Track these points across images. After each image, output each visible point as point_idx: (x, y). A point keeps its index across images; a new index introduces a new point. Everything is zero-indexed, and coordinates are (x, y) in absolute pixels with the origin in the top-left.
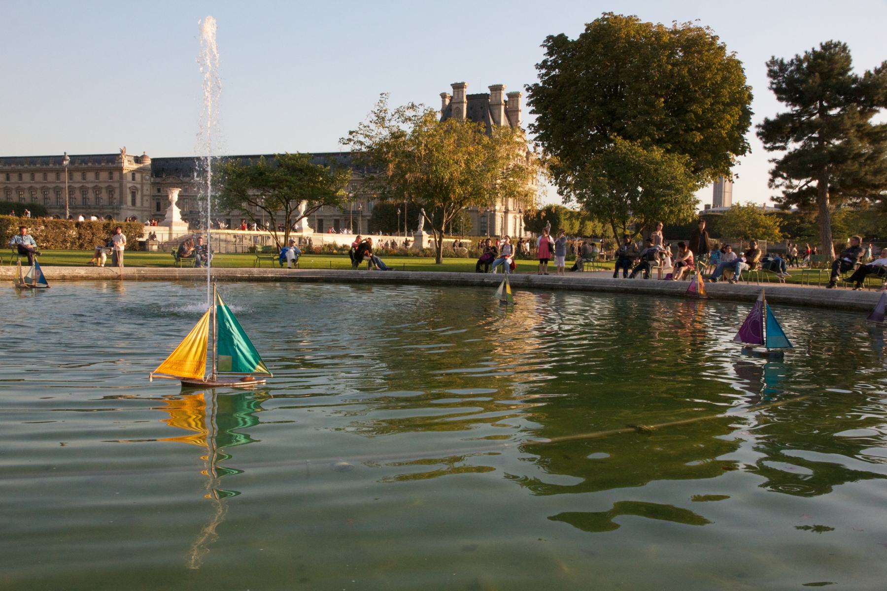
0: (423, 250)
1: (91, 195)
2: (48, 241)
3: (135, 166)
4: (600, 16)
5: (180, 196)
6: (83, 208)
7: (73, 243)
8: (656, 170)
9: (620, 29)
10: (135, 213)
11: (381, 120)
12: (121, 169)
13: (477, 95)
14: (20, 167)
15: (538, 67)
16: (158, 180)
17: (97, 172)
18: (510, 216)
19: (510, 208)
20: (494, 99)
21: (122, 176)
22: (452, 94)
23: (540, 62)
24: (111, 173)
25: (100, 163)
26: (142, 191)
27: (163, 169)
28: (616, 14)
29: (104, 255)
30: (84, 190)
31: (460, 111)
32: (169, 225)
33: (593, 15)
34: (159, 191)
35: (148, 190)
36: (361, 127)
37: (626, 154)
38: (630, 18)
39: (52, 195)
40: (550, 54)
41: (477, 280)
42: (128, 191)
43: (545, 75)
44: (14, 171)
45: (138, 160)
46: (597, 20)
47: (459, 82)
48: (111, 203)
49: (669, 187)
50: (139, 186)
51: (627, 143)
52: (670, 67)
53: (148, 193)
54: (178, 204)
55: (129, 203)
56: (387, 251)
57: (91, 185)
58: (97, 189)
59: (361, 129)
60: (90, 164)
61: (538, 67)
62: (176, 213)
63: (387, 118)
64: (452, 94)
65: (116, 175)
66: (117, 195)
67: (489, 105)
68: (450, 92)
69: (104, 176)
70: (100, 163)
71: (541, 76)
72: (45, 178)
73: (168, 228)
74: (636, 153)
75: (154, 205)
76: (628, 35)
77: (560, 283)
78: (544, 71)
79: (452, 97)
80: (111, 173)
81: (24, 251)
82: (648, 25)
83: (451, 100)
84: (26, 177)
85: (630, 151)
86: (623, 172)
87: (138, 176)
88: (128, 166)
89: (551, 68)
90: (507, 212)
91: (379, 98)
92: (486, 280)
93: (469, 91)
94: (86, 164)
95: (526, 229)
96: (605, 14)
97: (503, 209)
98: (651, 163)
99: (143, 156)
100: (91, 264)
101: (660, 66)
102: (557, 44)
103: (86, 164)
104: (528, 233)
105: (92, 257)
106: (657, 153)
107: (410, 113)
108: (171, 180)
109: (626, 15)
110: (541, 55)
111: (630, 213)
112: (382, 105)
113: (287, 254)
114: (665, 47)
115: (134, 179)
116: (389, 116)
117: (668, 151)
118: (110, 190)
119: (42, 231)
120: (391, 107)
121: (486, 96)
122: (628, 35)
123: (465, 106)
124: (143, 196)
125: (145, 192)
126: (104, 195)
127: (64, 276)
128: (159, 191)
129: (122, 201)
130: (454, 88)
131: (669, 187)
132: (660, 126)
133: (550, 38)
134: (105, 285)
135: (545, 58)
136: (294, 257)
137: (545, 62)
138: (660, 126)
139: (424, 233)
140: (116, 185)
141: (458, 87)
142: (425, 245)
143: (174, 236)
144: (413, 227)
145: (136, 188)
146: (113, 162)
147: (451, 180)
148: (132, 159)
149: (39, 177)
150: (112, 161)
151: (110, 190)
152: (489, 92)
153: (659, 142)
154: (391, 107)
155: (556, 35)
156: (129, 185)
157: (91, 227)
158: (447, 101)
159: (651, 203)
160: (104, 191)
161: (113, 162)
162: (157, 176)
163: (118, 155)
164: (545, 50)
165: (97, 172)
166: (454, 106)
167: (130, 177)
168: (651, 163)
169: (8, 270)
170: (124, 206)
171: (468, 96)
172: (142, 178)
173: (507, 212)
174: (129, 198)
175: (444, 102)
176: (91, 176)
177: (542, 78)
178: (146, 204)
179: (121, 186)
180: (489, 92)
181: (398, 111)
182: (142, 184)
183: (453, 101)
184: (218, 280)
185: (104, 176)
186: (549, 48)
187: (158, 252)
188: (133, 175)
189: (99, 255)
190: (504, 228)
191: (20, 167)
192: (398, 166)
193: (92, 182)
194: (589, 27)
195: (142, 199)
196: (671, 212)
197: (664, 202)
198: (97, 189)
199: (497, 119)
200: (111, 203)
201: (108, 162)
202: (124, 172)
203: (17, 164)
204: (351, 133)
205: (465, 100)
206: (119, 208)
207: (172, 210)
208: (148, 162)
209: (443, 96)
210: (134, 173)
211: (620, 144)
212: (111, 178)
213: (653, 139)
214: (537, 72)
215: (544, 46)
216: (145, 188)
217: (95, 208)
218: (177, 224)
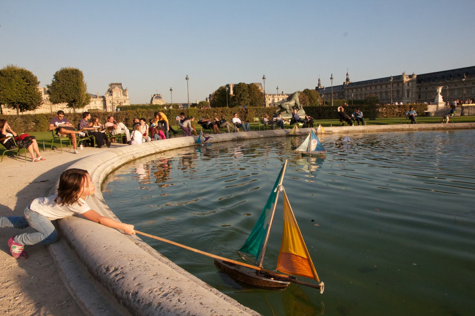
3: (409, 79)
5: (442, 90)
7: (397, 114)
10: (409, 101)
12: (403, 81)
14: (361, 86)
16: (420, 85)
24: (398, 84)
25: (382, 81)
26: (412, 90)
27: (422, 80)
29: (448, 118)
30: (386, 92)
32: (437, 104)
34: (420, 89)
35: (415, 89)
39: (384, 95)
42: (406, 91)
44: (359, 87)
45: (410, 77)
48: (398, 97)
50: (410, 88)
53: (415, 91)
54: (441, 94)
55: (406, 96)
57: (374, 92)
58: (381, 93)
62: (440, 98)
65: (401, 85)
66: (401, 93)
72: (371, 89)
75: (418, 96)
80: (398, 84)
81: (411, 117)
84: (364, 89)
87: (410, 84)
88: (406, 79)
99: (413, 75)
105: (441, 119)
108: (440, 82)
115: (408, 85)
118: (398, 92)
124: (412, 92)
125: (414, 91)
128: (420, 89)
129: (403, 95)
134: (447, 132)
140: (400, 89)
144: (210, 129)
145: (409, 89)
148: (408, 77)
149: (373, 88)
151: (398, 92)
156: (406, 88)
161: (399, 79)
162: (419, 83)
167: (406, 84)
172: (412, 85)
174: (406, 94)
176: (379, 87)
178: (414, 96)
179: (403, 89)
187: (435, 116)
189: (445, 118)
191: (361, 86)
195: (412, 94)
198: (381, 93)
200: (398, 97)
201: (397, 79)
203: (360, 84)
207: (438, 97)
210: (408, 82)
212: (398, 86)
216: (413, 89)
218: (441, 103)
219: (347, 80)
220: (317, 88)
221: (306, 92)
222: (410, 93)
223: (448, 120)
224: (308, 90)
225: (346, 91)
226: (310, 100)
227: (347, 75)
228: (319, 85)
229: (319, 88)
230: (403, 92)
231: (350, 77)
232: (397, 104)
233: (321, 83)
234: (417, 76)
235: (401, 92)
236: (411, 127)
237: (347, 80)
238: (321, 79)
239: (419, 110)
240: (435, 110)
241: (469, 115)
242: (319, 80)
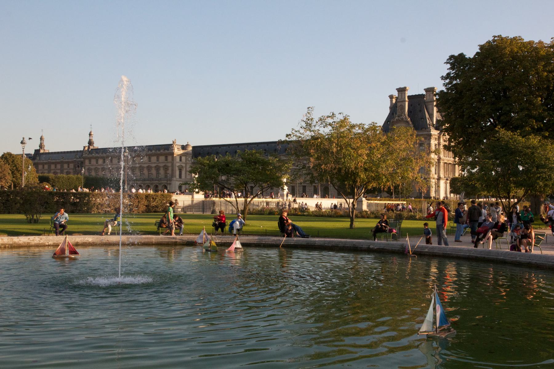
0: (361, 211)
1: (154, 172)
2: (110, 207)
3: (182, 152)
4: (491, 39)
6: (148, 180)
8: (533, 153)
9: (505, 48)
11: (308, 126)
12: (173, 154)
13: (416, 95)
14: (158, 152)
15: (443, 78)
17: (158, 156)
18: (442, 183)
19: (442, 175)
20: (428, 97)
21: (173, 157)
22: (397, 96)
23: (445, 75)
24: (166, 157)
25: (159, 150)
28: (503, 36)
29: (110, 226)
30: (157, 168)
31: (403, 108)
33: (485, 38)
36: (293, 131)
37: (508, 141)
38: (515, 38)
40: (452, 68)
41: (365, 246)
42: (177, 168)
43: (448, 84)
45: (184, 147)
46: (489, 42)
47: (402, 87)
48: (166, 176)
49: (544, 166)
50: (184, 165)
51: (509, 133)
52: (546, 74)
55: (178, 176)
56: (336, 213)
57: (153, 165)
58: (149, 168)
59: (293, 133)
60: (153, 151)
61: (443, 78)
63: (313, 125)
64: (397, 96)
65: (170, 158)
66: (169, 172)
67: (425, 102)
68: (396, 94)
69: (162, 158)
70: (159, 150)
71: (445, 85)
73: (191, 196)
74: (515, 141)
76: (512, 51)
77: (426, 250)
78: (448, 81)
79: (397, 98)
80: (166, 157)
82: (531, 43)
83: (396, 100)
85: (511, 139)
86: (506, 155)
87: (183, 158)
88: (177, 151)
89: (454, 78)
90: (439, 179)
91: (306, 111)
92: (371, 247)
93: (409, 93)
94: (151, 151)
95: (451, 192)
96: (495, 37)
97: (436, 176)
98: (528, 148)
99: (187, 145)
100: (100, 234)
101: (537, 73)
102: (457, 61)
103: (151, 151)
104: (452, 195)
106: (534, 140)
107: (330, 120)
109: (511, 36)
110: (445, 69)
111: (512, 185)
112: (309, 115)
113: (234, 225)
114: (542, 58)
115: (181, 160)
116: (314, 123)
117: (545, 137)
118: (166, 168)
119: (106, 200)
120: (316, 117)
121: (422, 96)
122: (512, 51)
123: (407, 104)
124: (186, 171)
126: (162, 171)
127: (77, 243)
129: (173, 175)
130: (398, 91)
131: (544, 166)
132: (540, 119)
133: (452, 57)
135: (448, 71)
136: (239, 228)
137: (448, 74)
138: (540, 119)
139: (364, 199)
140: (169, 165)
141: (402, 90)
142: (365, 207)
143: (194, 202)
145: (182, 167)
146: (168, 150)
147: (356, 168)
148: (180, 147)
150: (167, 149)
151: (166, 168)
152: (424, 93)
153: (537, 131)
154: (316, 117)
155: (456, 54)
156: (178, 164)
157: (137, 197)
158: (394, 101)
159: (530, 178)
160: (162, 169)
161: (168, 150)
163: (171, 145)
164: (449, 66)
165: (158, 156)
166: (399, 104)
167: (178, 159)
168: (528, 148)
169: (41, 239)
170: (174, 179)
171: (409, 97)
172: (186, 159)
173: (439, 179)
175: (391, 101)
177: (446, 86)
180: (424, 93)
181: (321, 120)
182: (186, 164)
183: (398, 100)
184: (53, 285)
185: (162, 158)
186: (451, 64)
188: (181, 157)
190: (437, 191)
191: (158, 152)
192: (318, 158)
193: (155, 163)
194: (482, 47)
195: (186, 174)
196: (546, 185)
197: (539, 178)
198: (157, 168)
199: (430, 112)
200: (166, 176)
202: (175, 155)
204: (287, 136)
205: (407, 99)
206: (171, 180)
208: (190, 149)
209: (391, 97)
210: (181, 156)
211: (504, 133)
212: (166, 160)
213: (533, 128)
214: (443, 82)
215: (447, 63)
217: (156, 180)
219: (90, 143)
220: (37, 151)
221: (6, 158)
222: (183, 172)
223: (110, 230)
224: (10, 154)
225: (87, 162)
226: (12, 172)
227: (90, 135)
228: (41, 146)
229: (42, 151)
230: (173, 170)
231: (94, 139)
232: (134, 190)
233: (45, 143)
234: (193, 147)
235: (170, 169)
236: (42, 242)
237: (90, 143)
238: (44, 137)
239: (159, 202)
240: (190, 203)
241: (232, 214)
242: (41, 139)
